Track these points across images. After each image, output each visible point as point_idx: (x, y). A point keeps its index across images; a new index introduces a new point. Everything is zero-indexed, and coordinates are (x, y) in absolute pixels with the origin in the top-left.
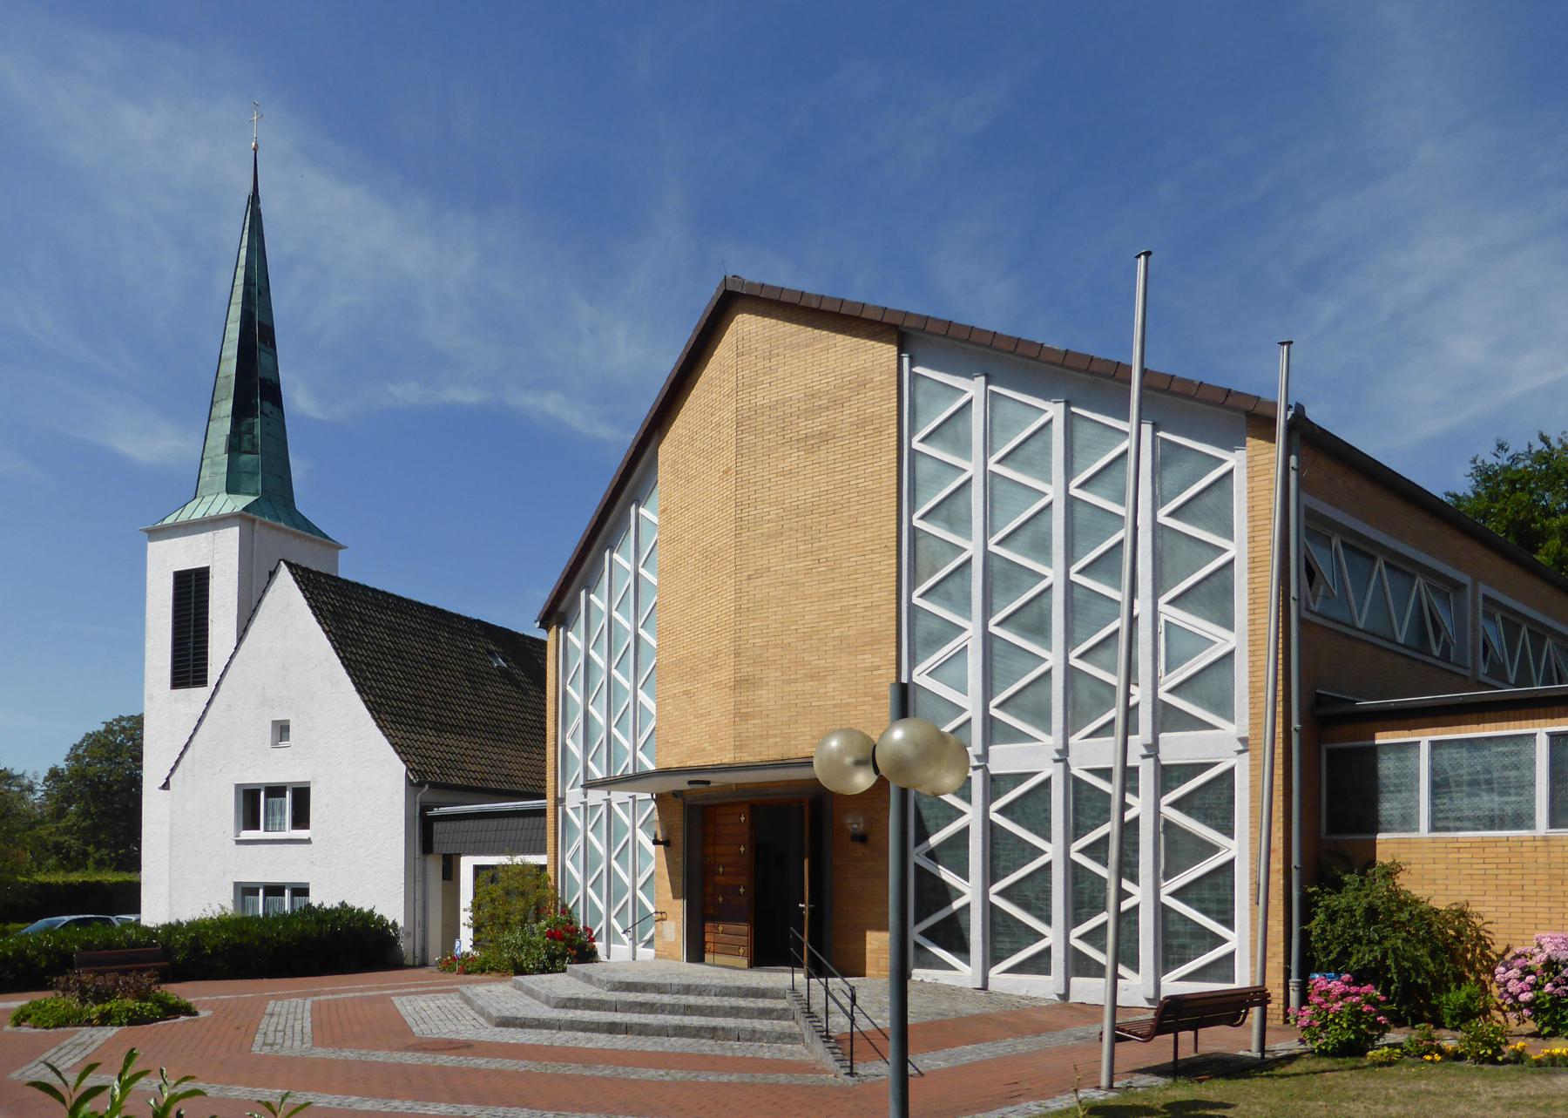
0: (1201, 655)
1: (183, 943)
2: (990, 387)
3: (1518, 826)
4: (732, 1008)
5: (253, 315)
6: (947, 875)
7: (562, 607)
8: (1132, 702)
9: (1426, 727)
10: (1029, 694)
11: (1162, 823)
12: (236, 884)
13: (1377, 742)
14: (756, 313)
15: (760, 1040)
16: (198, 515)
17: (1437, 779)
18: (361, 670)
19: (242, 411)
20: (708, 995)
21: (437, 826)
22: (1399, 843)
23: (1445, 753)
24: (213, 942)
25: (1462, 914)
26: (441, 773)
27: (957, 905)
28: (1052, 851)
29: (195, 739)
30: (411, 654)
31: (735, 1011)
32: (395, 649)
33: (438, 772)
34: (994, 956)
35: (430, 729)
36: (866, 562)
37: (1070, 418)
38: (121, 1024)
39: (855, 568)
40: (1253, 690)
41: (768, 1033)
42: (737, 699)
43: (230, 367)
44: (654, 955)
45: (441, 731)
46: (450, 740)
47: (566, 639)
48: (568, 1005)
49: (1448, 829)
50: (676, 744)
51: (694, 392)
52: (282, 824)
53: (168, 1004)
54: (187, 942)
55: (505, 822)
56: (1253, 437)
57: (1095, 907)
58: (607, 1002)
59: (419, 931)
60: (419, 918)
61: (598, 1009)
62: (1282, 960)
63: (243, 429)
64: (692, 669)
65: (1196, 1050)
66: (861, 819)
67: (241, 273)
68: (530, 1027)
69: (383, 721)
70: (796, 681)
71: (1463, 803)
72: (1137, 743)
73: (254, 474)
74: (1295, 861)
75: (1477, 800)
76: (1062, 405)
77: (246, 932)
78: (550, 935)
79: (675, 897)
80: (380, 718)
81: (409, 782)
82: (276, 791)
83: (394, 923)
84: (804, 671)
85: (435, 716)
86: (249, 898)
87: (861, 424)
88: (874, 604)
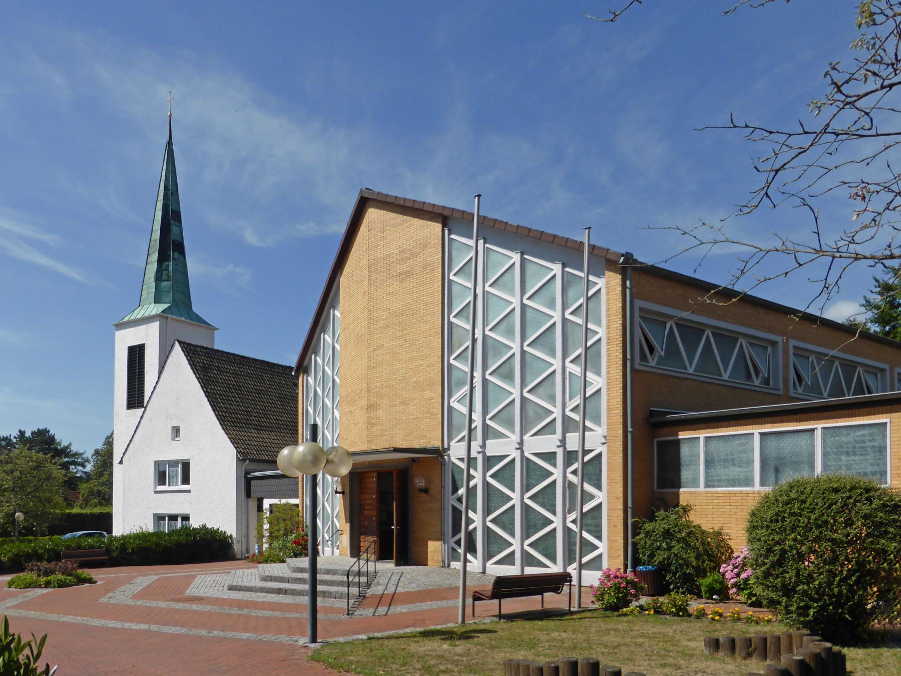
1: (117, 547)
2: (486, 245)
3: (747, 486)
5: (168, 206)
7: (305, 364)
8: (473, 426)
10: (505, 411)
11: (567, 482)
12: (154, 515)
16: (139, 316)
17: (708, 458)
18: (216, 398)
19: (163, 258)
20: (338, 575)
21: (253, 483)
23: (713, 444)
24: (132, 546)
25: (719, 533)
26: (257, 454)
28: (515, 496)
29: (135, 436)
30: (247, 388)
32: (237, 385)
33: (255, 453)
34: (488, 556)
35: (253, 429)
37: (523, 261)
38: (54, 587)
40: (609, 410)
43: (157, 235)
45: (259, 430)
46: (265, 435)
49: (714, 486)
50: (346, 439)
51: (353, 250)
52: (177, 482)
53: (80, 578)
54: (119, 546)
56: (608, 271)
57: (537, 529)
58: (285, 578)
59: (244, 540)
60: (244, 532)
61: (281, 582)
62: (622, 559)
63: (163, 268)
65: (543, 606)
66: (424, 481)
67: (163, 184)
68: (243, 590)
69: (225, 426)
70: (395, 405)
71: (720, 472)
72: (476, 446)
73: (169, 292)
74: (630, 504)
75: (727, 470)
76: (519, 254)
77: (149, 541)
78: (295, 542)
79: (346, 522)
80: (224, 424)
81: (238, 459)
82: (173, 464)
83: (231, 536)
85: (257, 421)
86: (161, 522)
87: (425, 267)
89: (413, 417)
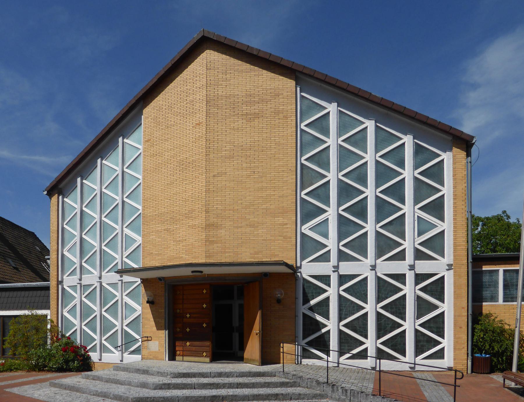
0: (432, 231)
4: (265, 383)
6: (319, 318)
9: (502, 265)
13: (483, 269)
14: (218, 51)
15: (303, 399)
22: (491, 306)
27: (324, 330)
31: (267, 385)
36: (279, 175)
39: (274, 178)
40: (455, 245)
41: (308, 395)
42: (207, 234)
44: (141, 358)
47: (63, 202)
48: (163, 387)
55: (11, 294)
61: (183, 388)
64: (171, 218)
70: (241, 227)
79: (158, 329)
84: (246, 223)
87: (277, 112)
88: (284, 195)
89: (263, 238)
